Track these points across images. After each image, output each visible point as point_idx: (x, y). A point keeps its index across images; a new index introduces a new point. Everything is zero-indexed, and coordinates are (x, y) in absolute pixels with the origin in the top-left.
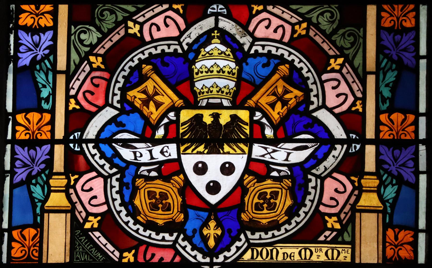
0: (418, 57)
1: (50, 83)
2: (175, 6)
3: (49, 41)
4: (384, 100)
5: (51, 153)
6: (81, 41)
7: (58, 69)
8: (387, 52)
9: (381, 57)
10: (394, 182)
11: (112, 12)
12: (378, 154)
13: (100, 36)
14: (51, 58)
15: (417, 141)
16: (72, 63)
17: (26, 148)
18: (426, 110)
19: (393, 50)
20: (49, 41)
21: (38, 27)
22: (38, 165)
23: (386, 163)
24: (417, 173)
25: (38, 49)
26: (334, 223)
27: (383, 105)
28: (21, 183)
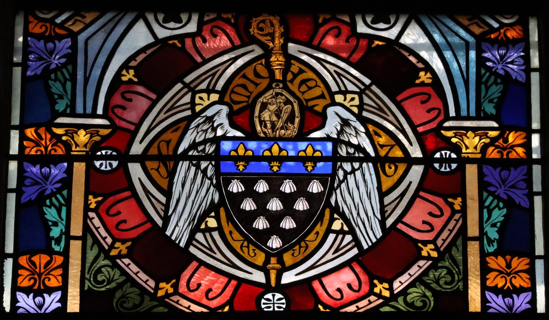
0: (528, 70)
2: (224, 16)
3: (56, 302)
4: (490, 242)
5: (69, 171)
7: (72, 234)
8: (492, 189)
9: (485, 194)
10: (501, 205)
12: (481, 175)
13: (425, 278)
14: (65, 193)
16: (460, 248)
17: (31, 296)
18: (541, 154)
20: (56, 302)
23: (491, 185)
24: (531, 195)
28: (30, 203)
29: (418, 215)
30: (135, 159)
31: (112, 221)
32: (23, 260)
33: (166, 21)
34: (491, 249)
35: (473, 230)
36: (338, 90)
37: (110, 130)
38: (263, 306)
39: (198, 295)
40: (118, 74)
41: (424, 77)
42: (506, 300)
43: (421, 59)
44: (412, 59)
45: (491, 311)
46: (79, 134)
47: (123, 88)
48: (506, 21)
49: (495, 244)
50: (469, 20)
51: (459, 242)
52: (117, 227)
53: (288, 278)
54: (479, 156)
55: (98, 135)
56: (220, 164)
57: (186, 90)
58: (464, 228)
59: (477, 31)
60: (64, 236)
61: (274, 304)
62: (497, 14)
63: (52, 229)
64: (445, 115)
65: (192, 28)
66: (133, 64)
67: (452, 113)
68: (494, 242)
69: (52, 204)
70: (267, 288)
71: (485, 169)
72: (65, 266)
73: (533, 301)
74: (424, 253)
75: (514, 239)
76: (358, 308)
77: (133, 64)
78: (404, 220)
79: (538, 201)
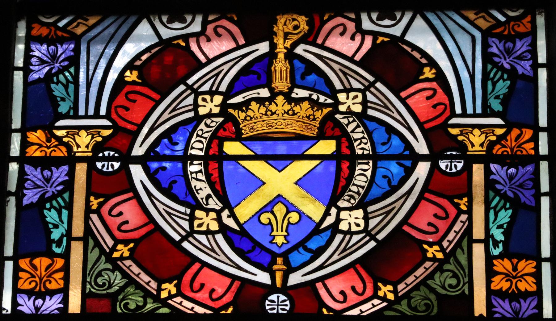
0: (536, 66)
1: (70, 97)
4: (496, 244)
5: (71, 174)
6: (455, 276)
9: (492, 194)
11: (415, 309)
12: (488, 172)
13: (429, 282)
15: (537, 158)
16: (465, 249)
17: (39, 169)
19: (503, 58)
21: (55, 37)
22: (55, 185)
25: (49, 185)
26: (436, 253)
27: (495, 249)
29: (425, 217)
30: (137, 160)
31: (442, 225)
32: (24, 263)
33: (170, 21)
34: (496, 252)
35: (478, 232)
36: (343, 88)
37: (111, 131)
38: (267, 307)
39: (202, 296)
40: (122, 74)
41: (428, 73)
42: (513, 303)
43: (424, 54)
44: (144, 58)
45: (497, 315)
46: (80, 134)
47: (127, 89)
48: (511, 14)
49: (501, 245)
50: (476, 14)
51: (465, 243)
52: (119, 229)
53: (295, 279)
54: (90, 154)
55: (100, 136)
56: (481, 163)
57: (189, 92)
58: (469, 231)
59: (483, 24)
60: (65, 239)
61: (278, 305)
62: (492, 8)
63: (52, 232)
64: (451, 111)
65: (196, 27)
66: (138, 63)
67: (458, 110)
68: (500, 243)
69: (52, 207)
70: (272, 289)
71: (494, 167)
72: (66, 269)
73: (540, 306)
74: (430, 255)
75: (520, 242)
76: (362, 312)
77: (138, 63)
78: (410, 221)
79: (545, 202)
